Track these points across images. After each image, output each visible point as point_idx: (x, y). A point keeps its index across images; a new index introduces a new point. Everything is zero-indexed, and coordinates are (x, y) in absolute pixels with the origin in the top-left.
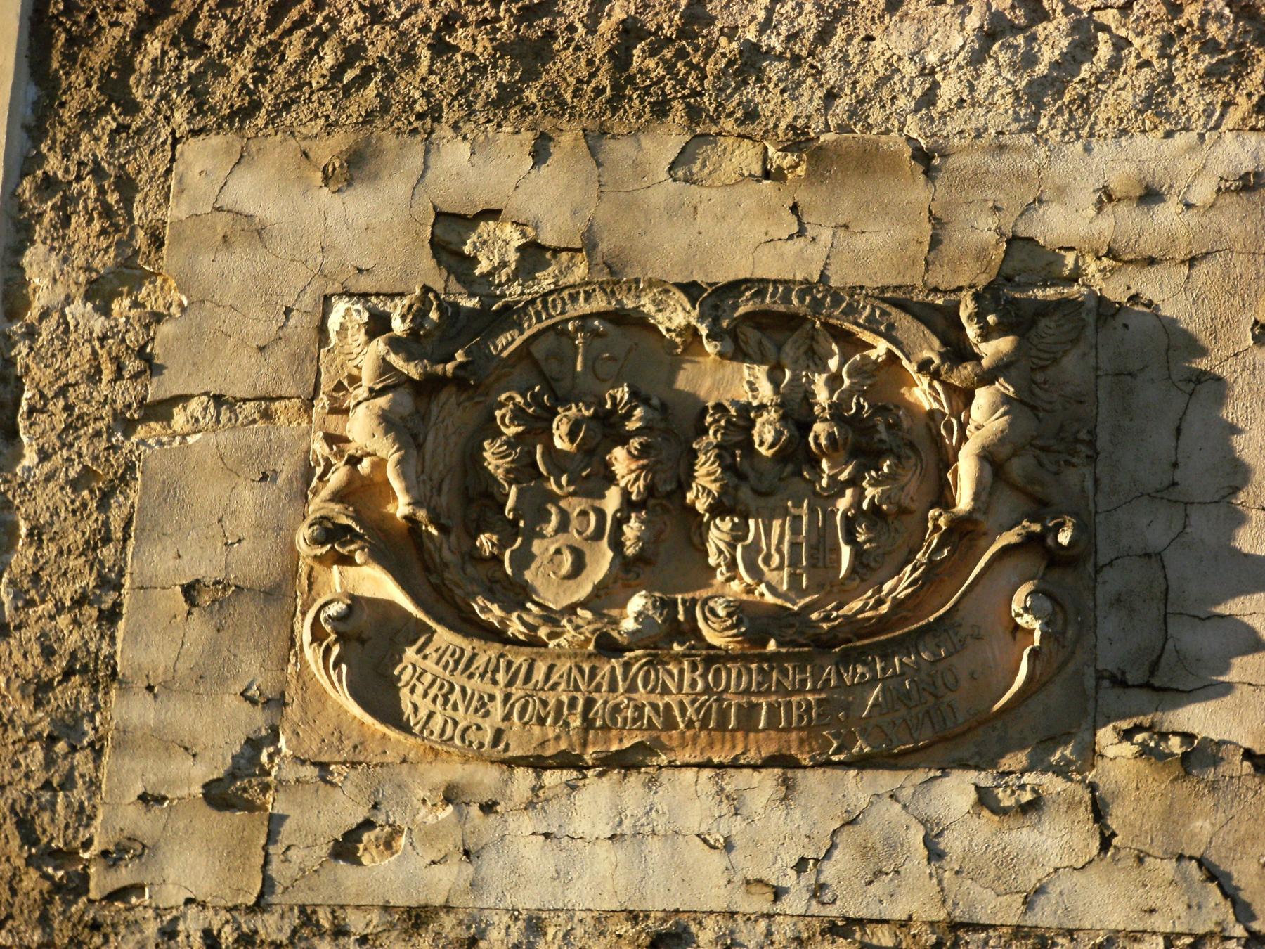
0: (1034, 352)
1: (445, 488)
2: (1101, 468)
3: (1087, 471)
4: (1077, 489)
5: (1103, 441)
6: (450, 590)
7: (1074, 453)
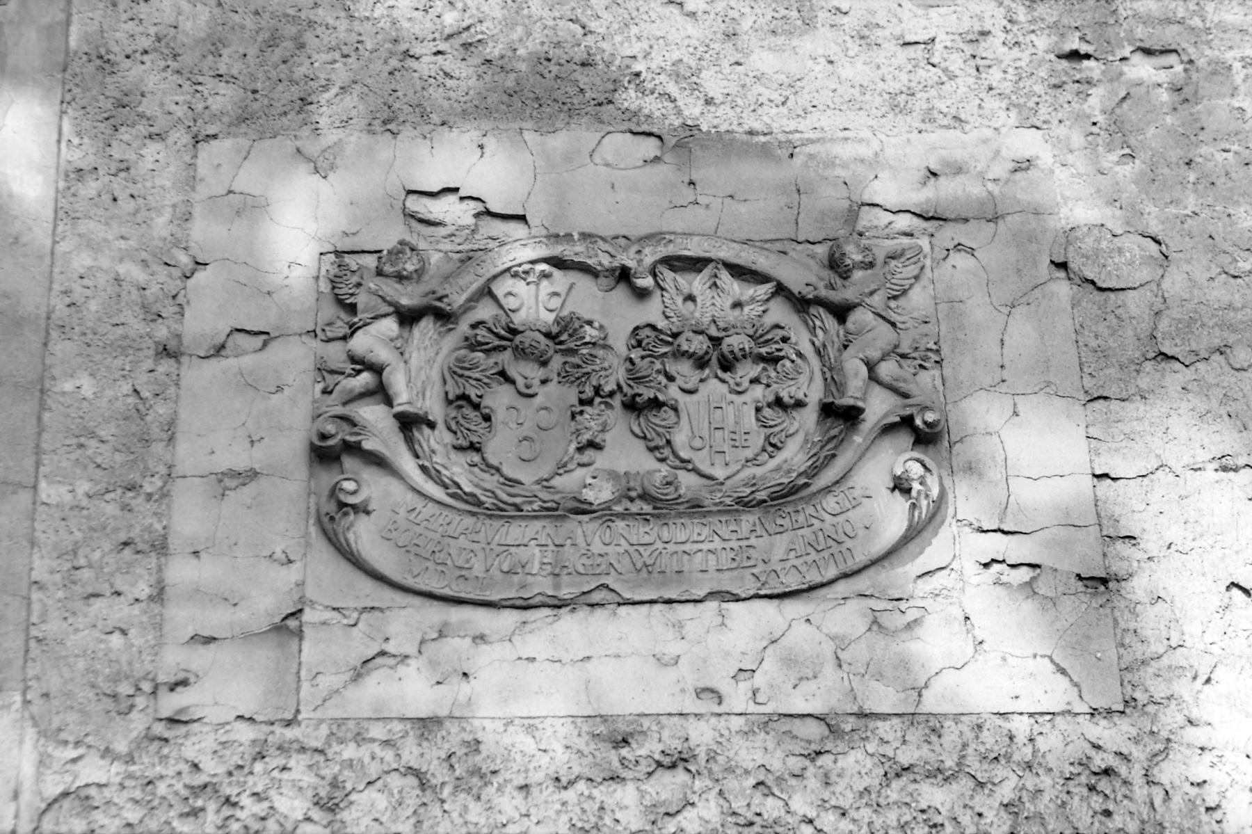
0: (888, 285)
1: (428, 393)
2: (947, 371)
3: (936, 373)
4: (930, 385)
5: (945, 350)
6: (438, 471)
7: (925, 359)
